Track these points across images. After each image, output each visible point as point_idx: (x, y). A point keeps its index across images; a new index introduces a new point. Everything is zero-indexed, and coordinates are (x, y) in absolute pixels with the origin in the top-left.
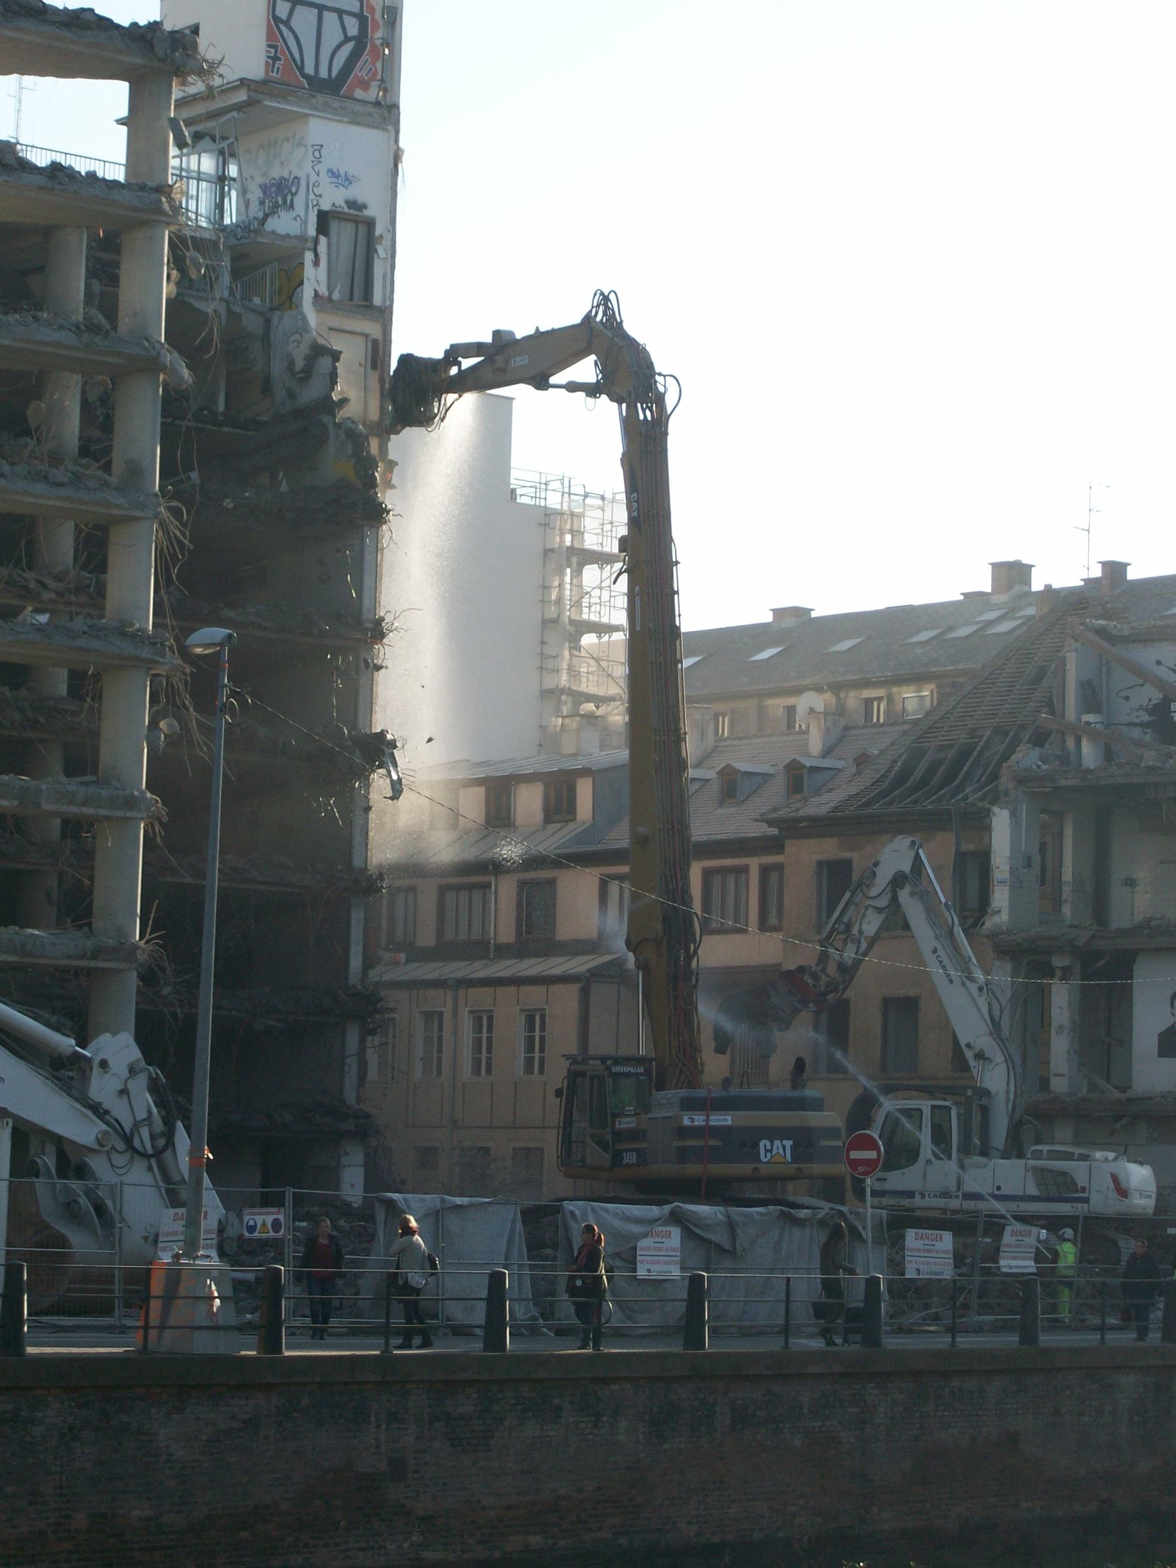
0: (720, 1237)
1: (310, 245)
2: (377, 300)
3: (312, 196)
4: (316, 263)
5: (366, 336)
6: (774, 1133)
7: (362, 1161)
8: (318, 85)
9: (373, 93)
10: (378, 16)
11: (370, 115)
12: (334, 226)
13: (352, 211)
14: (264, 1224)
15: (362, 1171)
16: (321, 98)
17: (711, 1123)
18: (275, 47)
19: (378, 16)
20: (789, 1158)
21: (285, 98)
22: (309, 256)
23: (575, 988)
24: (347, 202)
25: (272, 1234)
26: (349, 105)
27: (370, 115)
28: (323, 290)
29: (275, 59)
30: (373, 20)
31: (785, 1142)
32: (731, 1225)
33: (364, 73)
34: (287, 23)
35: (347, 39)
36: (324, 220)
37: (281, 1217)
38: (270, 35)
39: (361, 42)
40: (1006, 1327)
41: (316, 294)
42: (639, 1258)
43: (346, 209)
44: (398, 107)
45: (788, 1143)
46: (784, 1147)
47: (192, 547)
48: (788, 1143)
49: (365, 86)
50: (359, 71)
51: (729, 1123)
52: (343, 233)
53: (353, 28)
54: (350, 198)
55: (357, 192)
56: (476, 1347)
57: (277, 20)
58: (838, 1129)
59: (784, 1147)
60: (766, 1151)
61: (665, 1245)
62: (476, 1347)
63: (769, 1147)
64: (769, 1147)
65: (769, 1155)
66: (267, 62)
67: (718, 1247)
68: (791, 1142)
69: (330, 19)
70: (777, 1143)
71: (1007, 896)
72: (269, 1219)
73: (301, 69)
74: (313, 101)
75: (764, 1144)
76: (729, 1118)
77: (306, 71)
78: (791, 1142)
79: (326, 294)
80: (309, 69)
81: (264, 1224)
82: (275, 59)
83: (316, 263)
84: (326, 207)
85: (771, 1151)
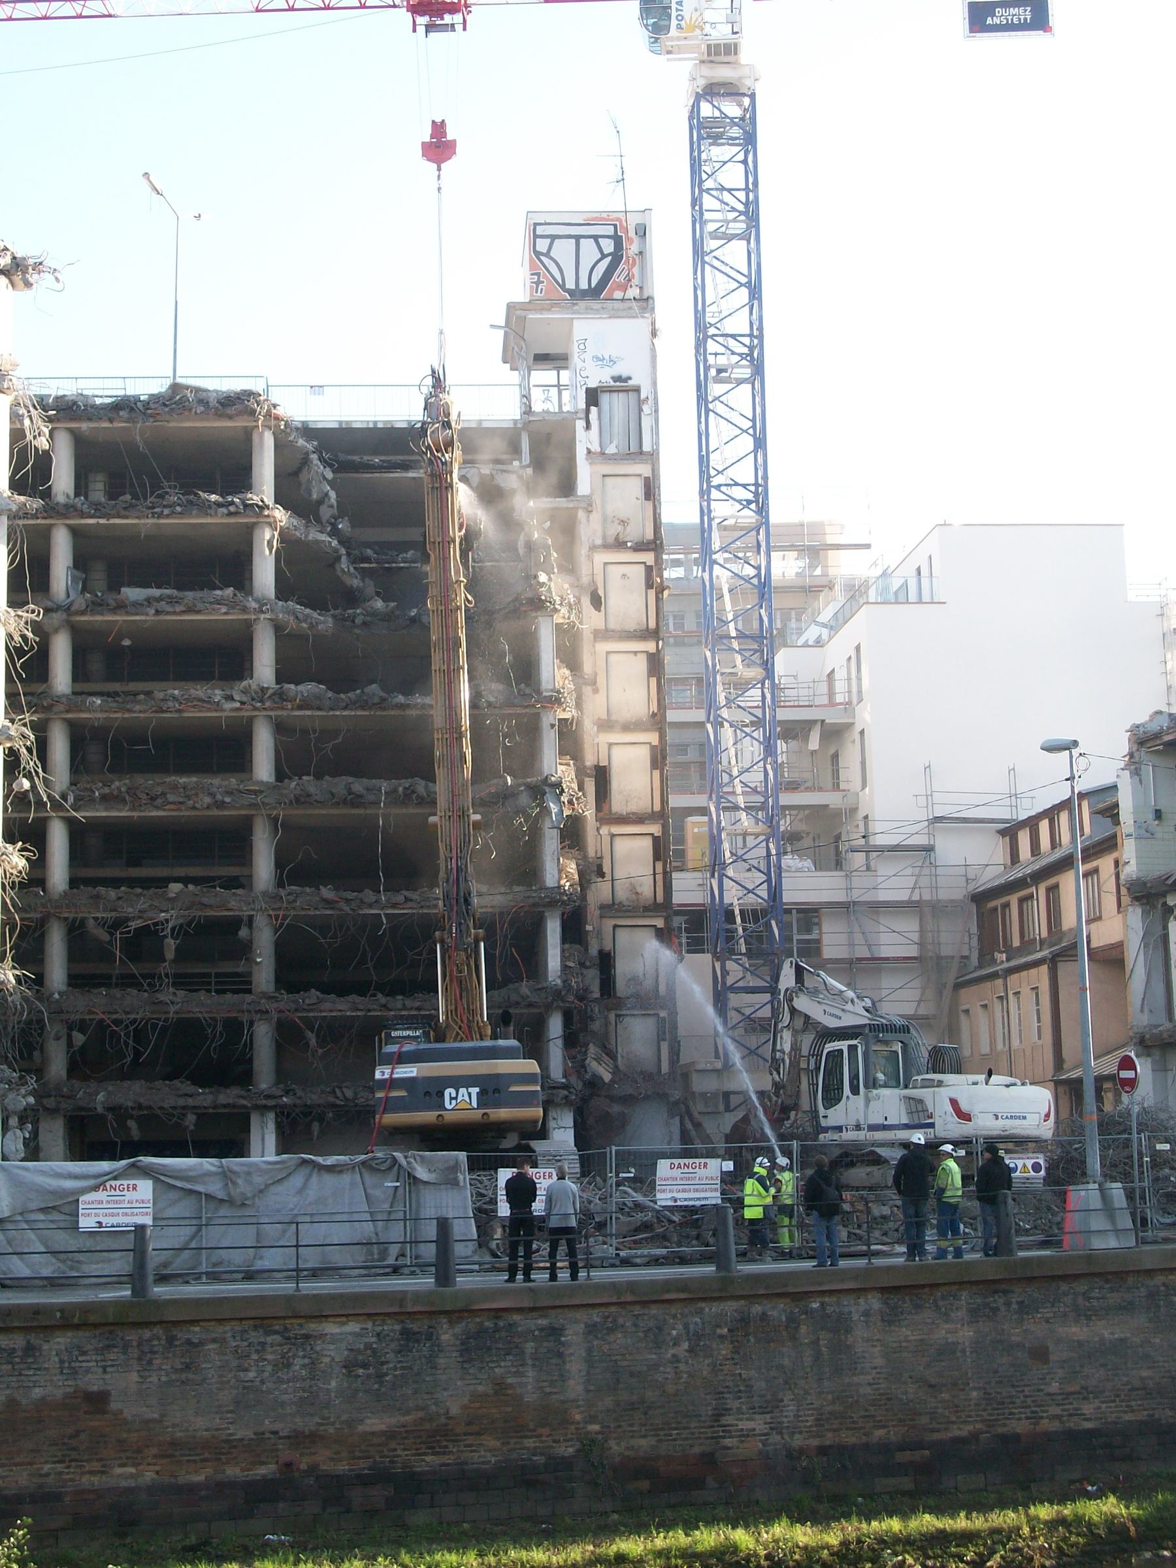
0: (215, 1188)
1: (583, 415)
2: (647, 447)
3: (579, 378)
4: (588, 426)
5: (640, 475)
6: (458, 1082)
7: (572, 1124)
8: (577, 295)
9: (633, 292)
10: (632, 233)
11: (630, 308)
12: (604, 399)
13: (618, 384)
14: (1024, 1166)
15: (572, 1131)
16: (582, 304)
17: (395, 1076)
18: (538, 274)
19: (632, 233)
20: (475, 1104)
21: (549, 310)
22: (580, 424)
23: (1044, 969)
24: (613, 378)
25: (1032, 1173)
26: (609, 304)
27: (630, 308)
28: (596, 448)
29: (538, 283)
30: (628, 238)
31: (470, 1090)
32: (227, 1176)
33: (622, 278)
34: (547, 255)
35: (604, 256)
36: (593, 397)
37: (1041, 1162)
38: (532, 265)
39: (617, 257)
40: (704, 1259)
41: (589, 451)
42: (81, 1211)
43: (612, 383)
44: (653, 298)
45: (475, 1091)
46: (470, 1094)
47: (37, 639)
48: (475, 1091)
49: (624, 288)
50: (618, 277)
51: (414, 1074)
52: (615, 404)
53: (608, 246)
54: (616, 374)
55: (620, 370)
56: (426, 1282)
57: (538, 254)
58: (535, 1074)
59: (470, 1094)
60: (451, 1099)
61: (126, 1198)
62: (426, 1282)
63: (454, 1095)
64: (454, 1095)
65: (454, 1102)
66: (531, 287)
67: (208, 1196)
68: (477, 1089)
69: (588, 246)
70: (463, 1091)
71: (1133, 848)
72: (1029, 1163)
73: (563, 286)
74: (576, 308)
75: (449, 1092)
76: (415, 1070)
77: (567, 287)
78: (477, 1089)
79: (599, 450)
80: (571, 285)
81: (1024, 1166)
82: (538, 283)
83: (588, 426)
84: (593, 384)
85: (456, 1098)
